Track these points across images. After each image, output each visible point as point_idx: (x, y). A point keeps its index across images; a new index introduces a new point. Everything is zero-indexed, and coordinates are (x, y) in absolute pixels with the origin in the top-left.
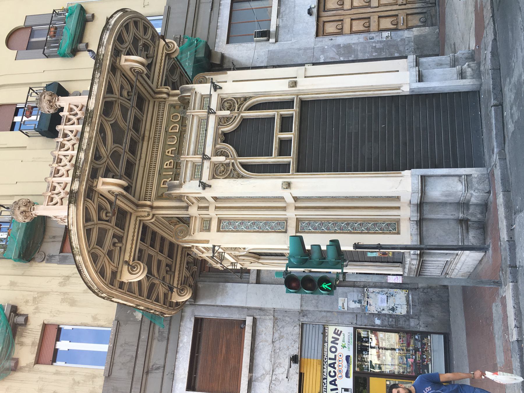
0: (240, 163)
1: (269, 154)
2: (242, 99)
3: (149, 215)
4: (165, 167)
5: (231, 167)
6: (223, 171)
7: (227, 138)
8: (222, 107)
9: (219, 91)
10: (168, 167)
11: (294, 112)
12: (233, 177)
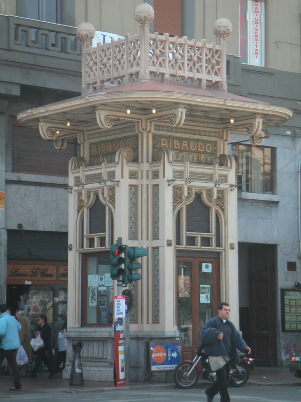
0: (182, 208)
1: (188, 230)
2: (223, 207)
3: (143, 129)
4: (175, 141)
5: (180, 201)
6: (177, 194)
7: (198, 196)
8: (219, 192)
9: (229, 188)
10: (175, 144)
11: (213, 247)
12: (174, 203)
